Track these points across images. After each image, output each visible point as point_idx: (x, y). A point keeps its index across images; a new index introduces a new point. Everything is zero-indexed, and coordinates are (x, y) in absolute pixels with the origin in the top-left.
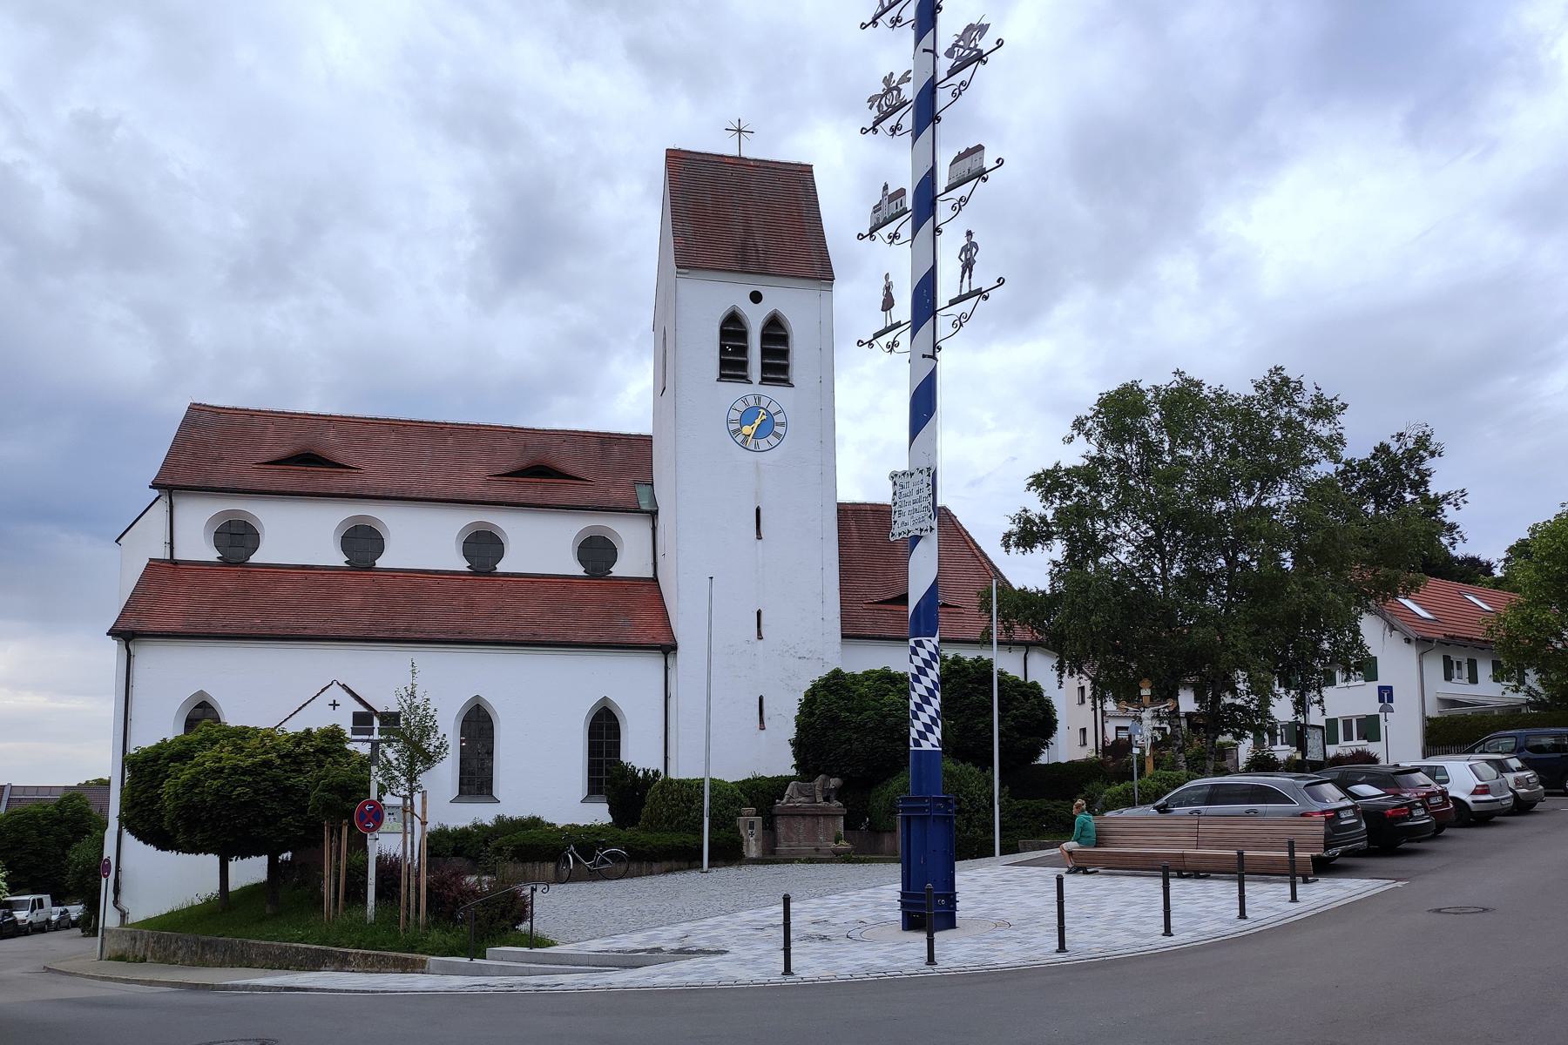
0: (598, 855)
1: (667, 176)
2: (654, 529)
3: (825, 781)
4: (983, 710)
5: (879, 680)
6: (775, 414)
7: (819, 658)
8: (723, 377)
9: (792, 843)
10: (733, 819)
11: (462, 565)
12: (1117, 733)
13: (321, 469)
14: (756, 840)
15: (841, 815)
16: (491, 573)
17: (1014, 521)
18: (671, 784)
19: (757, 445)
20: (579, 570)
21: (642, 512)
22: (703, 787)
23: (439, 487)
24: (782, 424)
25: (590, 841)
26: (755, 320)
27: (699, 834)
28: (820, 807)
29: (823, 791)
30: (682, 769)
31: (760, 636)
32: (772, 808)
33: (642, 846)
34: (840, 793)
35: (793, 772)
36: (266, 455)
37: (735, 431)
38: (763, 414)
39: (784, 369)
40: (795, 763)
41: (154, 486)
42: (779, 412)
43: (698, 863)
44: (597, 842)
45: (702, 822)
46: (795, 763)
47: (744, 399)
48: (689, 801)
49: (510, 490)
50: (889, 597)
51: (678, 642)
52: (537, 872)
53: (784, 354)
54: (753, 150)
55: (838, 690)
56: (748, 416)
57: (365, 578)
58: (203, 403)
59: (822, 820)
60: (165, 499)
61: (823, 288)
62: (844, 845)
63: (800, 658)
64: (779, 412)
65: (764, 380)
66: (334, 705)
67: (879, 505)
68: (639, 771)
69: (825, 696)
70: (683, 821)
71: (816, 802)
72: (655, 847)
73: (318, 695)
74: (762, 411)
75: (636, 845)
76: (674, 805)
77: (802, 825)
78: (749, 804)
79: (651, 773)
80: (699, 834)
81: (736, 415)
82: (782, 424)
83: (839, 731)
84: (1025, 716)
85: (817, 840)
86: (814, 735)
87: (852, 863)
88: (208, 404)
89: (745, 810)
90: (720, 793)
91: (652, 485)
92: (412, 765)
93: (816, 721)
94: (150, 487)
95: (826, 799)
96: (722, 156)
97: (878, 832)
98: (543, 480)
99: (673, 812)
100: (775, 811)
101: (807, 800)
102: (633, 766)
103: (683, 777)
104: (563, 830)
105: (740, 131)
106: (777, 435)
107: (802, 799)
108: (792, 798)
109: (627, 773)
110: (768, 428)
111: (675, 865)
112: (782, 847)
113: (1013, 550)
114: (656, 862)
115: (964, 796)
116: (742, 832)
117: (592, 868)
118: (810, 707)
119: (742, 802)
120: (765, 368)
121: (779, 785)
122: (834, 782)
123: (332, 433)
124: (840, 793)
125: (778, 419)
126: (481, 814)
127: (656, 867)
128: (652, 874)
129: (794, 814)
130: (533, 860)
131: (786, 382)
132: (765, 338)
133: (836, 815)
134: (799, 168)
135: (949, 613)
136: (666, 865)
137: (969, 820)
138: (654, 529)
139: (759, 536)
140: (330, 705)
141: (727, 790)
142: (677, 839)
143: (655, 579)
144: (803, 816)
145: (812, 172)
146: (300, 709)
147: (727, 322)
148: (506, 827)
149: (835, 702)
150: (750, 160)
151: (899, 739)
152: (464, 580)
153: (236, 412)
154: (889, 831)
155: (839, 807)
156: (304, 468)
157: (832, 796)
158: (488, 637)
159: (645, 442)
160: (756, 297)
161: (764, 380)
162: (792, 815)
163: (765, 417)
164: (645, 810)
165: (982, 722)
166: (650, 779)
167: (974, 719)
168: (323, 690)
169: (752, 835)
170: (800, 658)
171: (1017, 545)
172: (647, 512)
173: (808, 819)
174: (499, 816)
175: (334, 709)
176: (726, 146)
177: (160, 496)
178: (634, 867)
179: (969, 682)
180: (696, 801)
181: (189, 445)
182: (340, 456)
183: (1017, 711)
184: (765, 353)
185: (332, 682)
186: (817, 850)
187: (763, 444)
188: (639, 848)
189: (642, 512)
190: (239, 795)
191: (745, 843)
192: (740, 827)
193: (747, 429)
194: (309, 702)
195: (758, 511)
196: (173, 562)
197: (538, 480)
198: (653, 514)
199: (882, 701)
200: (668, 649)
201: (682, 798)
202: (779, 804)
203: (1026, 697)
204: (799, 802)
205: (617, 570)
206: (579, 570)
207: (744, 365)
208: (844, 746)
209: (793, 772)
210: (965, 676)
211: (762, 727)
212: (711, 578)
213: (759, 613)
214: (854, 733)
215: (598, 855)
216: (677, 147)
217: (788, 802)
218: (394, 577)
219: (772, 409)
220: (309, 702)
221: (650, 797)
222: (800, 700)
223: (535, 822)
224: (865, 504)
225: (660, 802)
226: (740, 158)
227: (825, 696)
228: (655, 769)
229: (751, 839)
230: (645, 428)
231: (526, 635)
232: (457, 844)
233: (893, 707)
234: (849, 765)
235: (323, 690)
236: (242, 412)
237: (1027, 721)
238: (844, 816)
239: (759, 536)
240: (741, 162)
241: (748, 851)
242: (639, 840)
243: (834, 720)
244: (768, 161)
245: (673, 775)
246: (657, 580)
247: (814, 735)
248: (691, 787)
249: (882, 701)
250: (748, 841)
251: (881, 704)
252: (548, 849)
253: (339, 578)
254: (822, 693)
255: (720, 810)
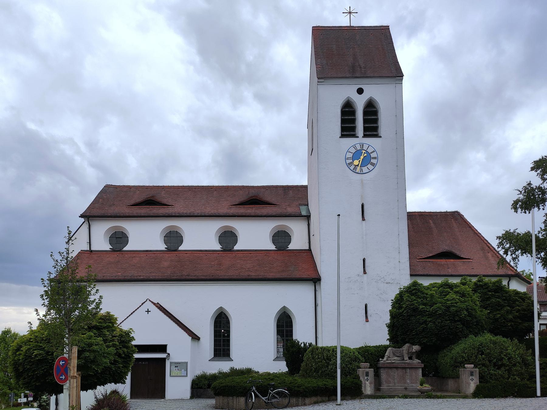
0: (270, 393)
1: (313, 39)
2: (309, 225)
3: (409, 347)
4: (499, 307)
5: (441, 287)
6: (371, 153)
7: (397, 283)
8: (343, 136)
9: (391, 385)
10: (354, 370)
11: (218, 247)
12: (540, 327)
13: (156, 207)
14: (370, 383)
15: (420, 368)
16: (231, 250)
17: (521, 192)
18: (317, 349)
19: (361, 170)
20: (273, 247)
21: (303, 216)
22: (336, 351)
23: (208, 210)
24: (375, 158)
25: (266, 384)
26: (360, 103)
27: (334, 379)
28: (407, 363)
29: (408, 353)
30: (326, 341)
31: (365, 272)
32: (377, 364)
33: (298, 387)
34: (419, 355)
35: (388, 343)
36: (133, 202)
37: (349, 164)
38: (365, 153)
39: (376, 129)
40: (389, 338)
41: (82, 216)
42: (374, 152)
43: (334, 397)
44: (269, 385)
45: (336, 372)
46: (389, 338)
47: (354, 146)
48: (328, 359)
49: (242, 210)
50: (431, 255)
51: (321, 276)
52: (235, 402)
53: (376, 121)
54: (356, 23)
55: (416, 293)
56: (356, 155)
57: (173, 255)
58: (111, 184)
59: (408, 370)
60: (87, 222)
61: (397, 82)
62: (427, 387)
63: (387, 283)
64: (374, 152)
65: (365, 136)
66: (148, 311)
67: (422, 212)
68: (301, 343)
69: (408, 296)
70: (325, 371)
71: (403, 360)
72: (306, 388)
73: (140, 306)
74: (364, 151)
75: (295, 387)
76: (319, 362)
77: (396, 374)
78: (364, 361)
79: (307, 344)
80: (334, 379)
81: (350, 155)
82: (375, 158)
83: (418, 317)
84: (524, 310)
85: (405, 383)
86: (403, 320)
87: (433, 398)
88: (113, 185)
89: (363, 364)
90: (346, 354)
91: (308, 205)
92: (40, 319)
93: (403, 311)
94: (80, 217)
95: (410, 358)
96: (341, 27)
97: (443, 378)
98: (255, 206)
99: (319, 366)
100: (380, 366)
101: (399, 359)
102: (298, 341)
103: (324, 345)
104: (262, 375)
105: (350, 13)
106: (373, 164)
107: (396, 358)
108: (390, 357)
109: (296, 344)
110: (368, 160)
111: (319, 398)
112: (384, 387)
113: (519, 210)
114: (308, 397)
115: (505, 355)
116: (361, 378)
117: (267, 401)
118: (399, 304)
119: (360, 360)
120: (365, 129)
121: (380, 351)
122: (416, 348)
123: (163, 192)
124: (419, 355)
125: (373, 155)
126: (224, 366)
127: (307, 400)
128: (305, 405)
129: (391, 367)
130: (233, 396)
131: (377, 136)
132: (365, 113)
133: (417, 368)
134: (382, 28)
135: (464, 262)
136: (314, 399)
137: (509, 371)
138: (309, 225)
139: (363, 219)
140: (146, 311)
141: (351, 352)
142: (320, 383)
143: (310, 250)
144: (397, 368)
145: (389, 29)
146: (132, 314)
147: (343, 108)
148: (234, 372)
149: (415, 300)
150: (356, 27)
151: (458, 321)
152: (218, 254)
153: (124, 187)
154: (453, 378)
155: (419, 363)
156: (148, 207)
157: (414, 357)
158: (226, 277)
159: (306, 187)
160: (360, 91)
161: (365, 136)
162: (391, 368)
163: (365, 155)
164: (303, 364)
165: (498, 314)
166: (307, 348)
167: (493, 312)
168: (142, 304)
169: (367, 380)
170: (387, 283)
171: (522, 208)
172: (305, 216)
173: (400, 370)
174: (231, 368)
175: (148, 313)
176: (343, 21)
177: (85, 221)
178: (293, 400)
179: (489, 291)
180: (332, 359)
181: (101, 200)
182: (165, 201)
183: (519, 307)
184: (365, 121)
185: (147, 300)
186: (406, 389)
187: (365, 169)
188: (296, 389)
189: (303, 216)
190: (36, 356)
191: (363, 385)
192: (360, 375)
193: (356, 162)
194: (136, 310)
195: (363, 206)
196: (91, 251)
197: (254, 206)
198: (308, 217)
199: (445, 299)
200: (316, 280)
201: (324, 357)
202: (382, 361)
203: (523, 300)
204: (394, 360)
205: (291, 247)
206: (273, 247)
207: (354, 129)
208: (422, 326)
209: (388, 343)
210: (487, 288)
211: (367, 321)
212: (339, 215)
213: (364, 260)
214: (428, 318)
215: (270, 393)
216: (318, 25)
217: (387, 360)
218: (186, 253)
219: (370, 150)
220: (136, 310)
221: (306, 357)
222: (392, 300)
223: (249, 371)
224: (415, 212)
225: (311, 360)
226: (350, 26)
227: (408, 296)
228: (310, 342)
229: (367, 382)
230: (305, 183)
231: (245, 274)
232: (210, 382)
233: (453, 301)
234: (425, 337)
235: (142, 304)
236: (127, 187)
237: (526, 312)
238: (422, 368)
239: (363, 219)
240: (351, 28)
241: (365, 390)
242: (296, 383)
243: (415, 310)
244: (365, 27)
245: (320, 345)
246: (311, 250)
247: (403, 320)
248: (329, 351)
249: (445, 299)
250: (365, 384)
251: (445, 300)
252: (240, 388)
253: (161, 255)
254: (407, 295)
255: (347, 365)
